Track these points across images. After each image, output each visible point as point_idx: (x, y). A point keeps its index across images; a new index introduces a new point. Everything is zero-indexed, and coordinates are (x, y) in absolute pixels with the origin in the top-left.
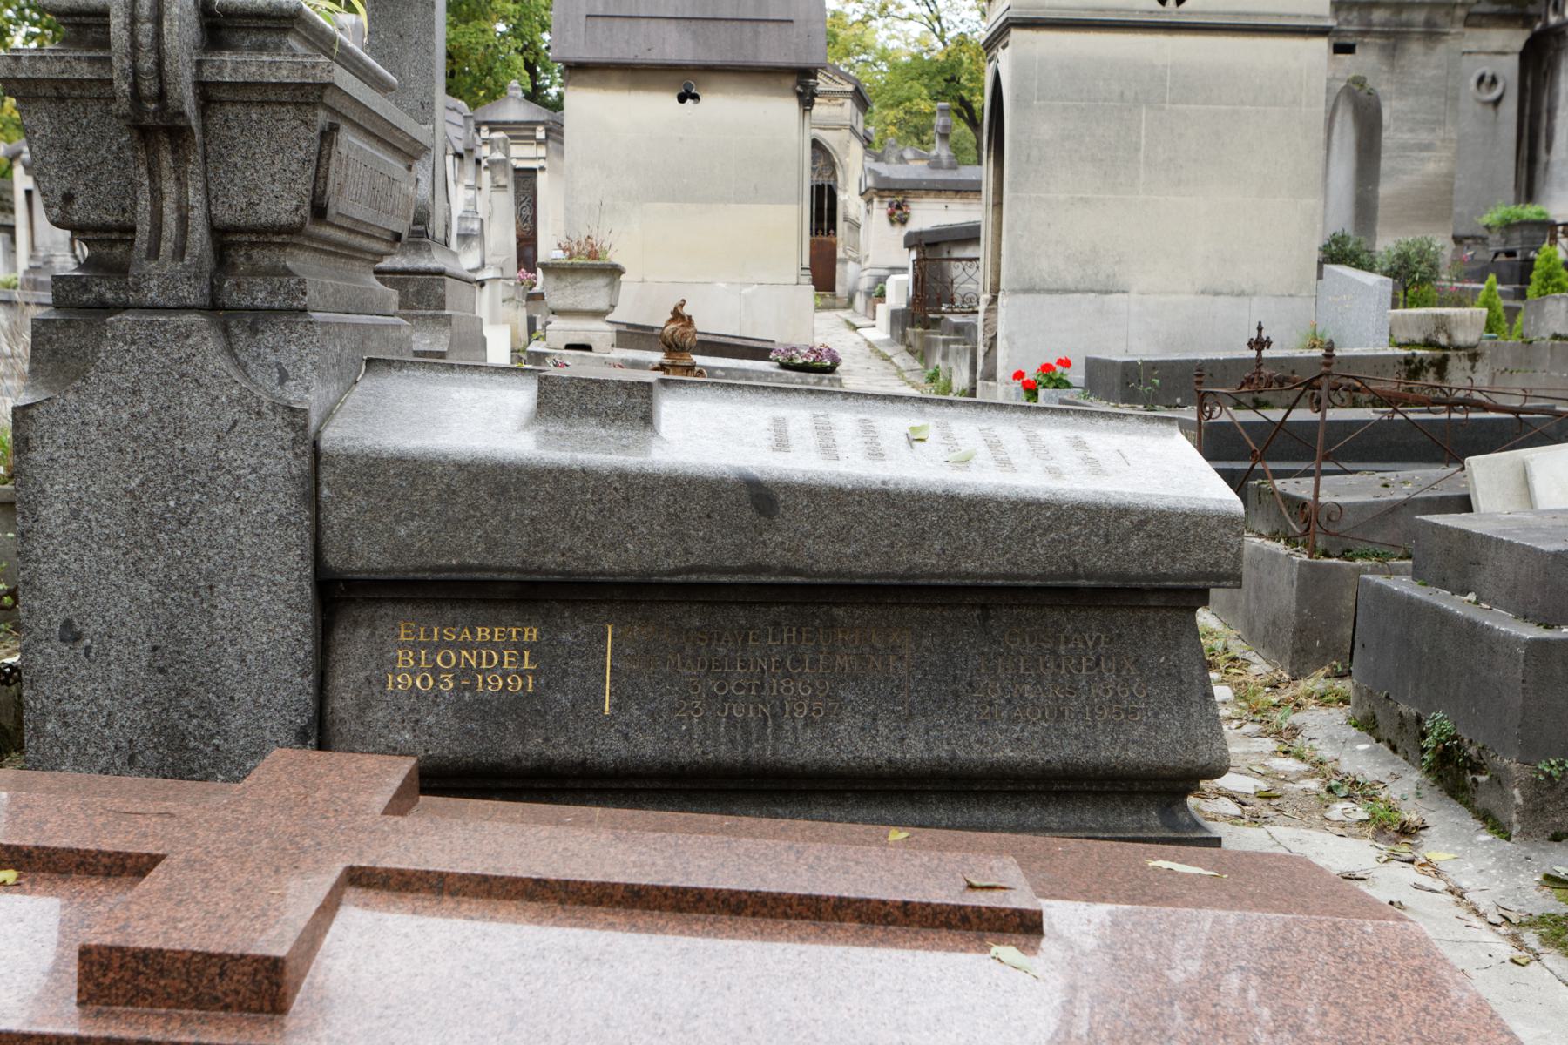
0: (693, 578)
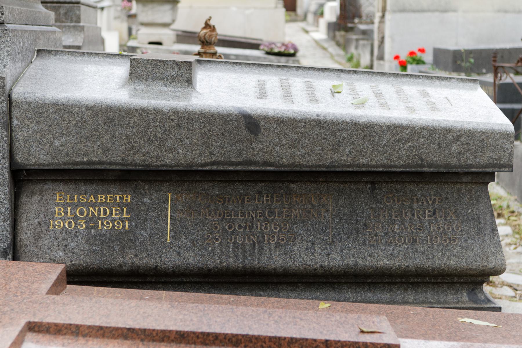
0: (215, 168)
